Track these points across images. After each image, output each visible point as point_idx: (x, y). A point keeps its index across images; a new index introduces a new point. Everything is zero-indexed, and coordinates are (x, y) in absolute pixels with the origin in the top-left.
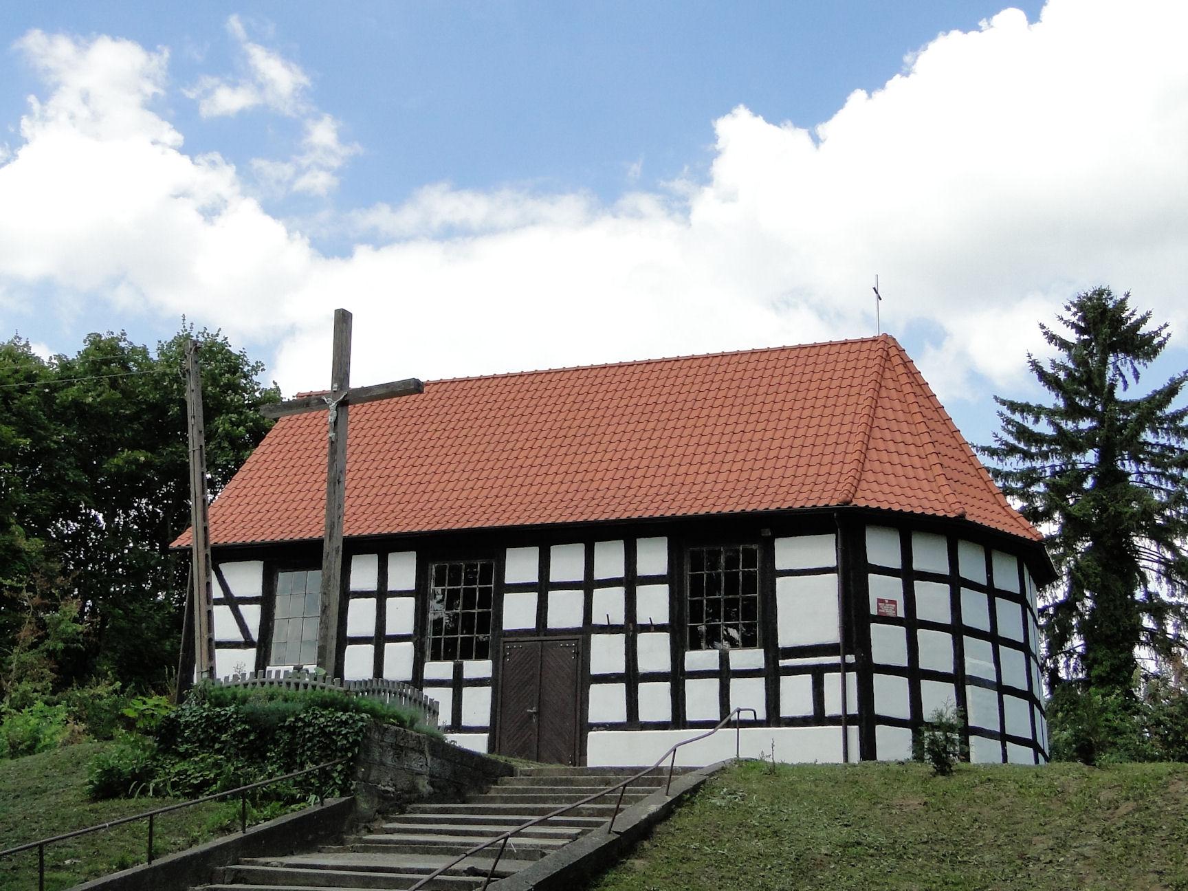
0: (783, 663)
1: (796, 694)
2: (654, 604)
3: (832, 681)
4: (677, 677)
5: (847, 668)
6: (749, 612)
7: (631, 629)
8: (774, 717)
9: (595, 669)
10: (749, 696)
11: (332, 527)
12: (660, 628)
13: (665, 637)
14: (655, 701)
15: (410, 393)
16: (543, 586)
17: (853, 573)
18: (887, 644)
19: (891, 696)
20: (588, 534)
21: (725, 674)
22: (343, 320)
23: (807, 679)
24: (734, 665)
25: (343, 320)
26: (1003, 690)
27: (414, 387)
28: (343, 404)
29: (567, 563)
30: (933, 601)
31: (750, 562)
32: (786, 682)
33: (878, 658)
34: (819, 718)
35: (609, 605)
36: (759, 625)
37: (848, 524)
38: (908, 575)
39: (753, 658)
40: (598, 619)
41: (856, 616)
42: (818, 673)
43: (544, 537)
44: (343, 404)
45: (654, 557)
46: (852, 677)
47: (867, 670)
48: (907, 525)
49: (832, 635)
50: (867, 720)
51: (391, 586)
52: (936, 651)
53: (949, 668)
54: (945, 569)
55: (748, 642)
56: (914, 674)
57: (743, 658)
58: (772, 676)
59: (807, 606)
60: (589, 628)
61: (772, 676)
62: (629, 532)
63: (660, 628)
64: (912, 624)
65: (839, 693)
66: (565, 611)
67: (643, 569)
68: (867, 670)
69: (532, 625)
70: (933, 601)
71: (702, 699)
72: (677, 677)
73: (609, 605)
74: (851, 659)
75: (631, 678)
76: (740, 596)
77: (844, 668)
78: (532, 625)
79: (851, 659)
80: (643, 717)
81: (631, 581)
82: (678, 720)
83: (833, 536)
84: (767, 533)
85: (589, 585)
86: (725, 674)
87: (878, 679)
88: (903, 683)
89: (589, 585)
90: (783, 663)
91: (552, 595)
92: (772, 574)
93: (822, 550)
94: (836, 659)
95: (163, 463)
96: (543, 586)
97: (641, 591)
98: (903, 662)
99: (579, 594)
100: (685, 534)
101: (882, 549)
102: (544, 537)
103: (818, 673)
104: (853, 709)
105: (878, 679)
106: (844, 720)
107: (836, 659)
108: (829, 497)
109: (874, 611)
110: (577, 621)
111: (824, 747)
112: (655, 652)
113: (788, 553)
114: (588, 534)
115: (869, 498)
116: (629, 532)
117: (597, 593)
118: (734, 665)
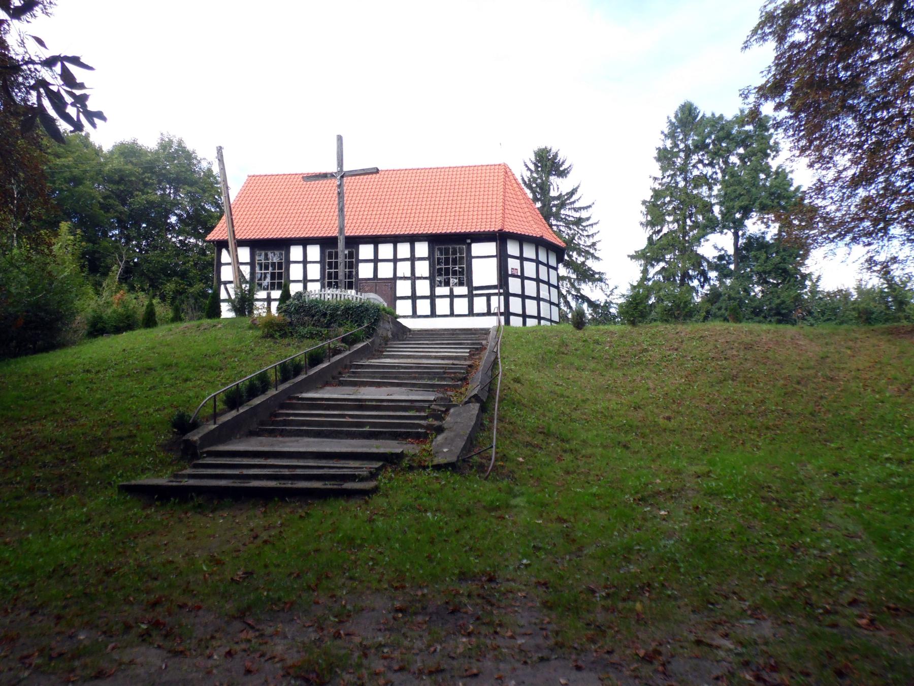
0: (475, 292)
1: (480, 304)
2: (423, 268)
3: (494, 300)
4: (432, 297)
5: (501, 294)
6: (461, 273)
7: (413, 278)
8: (471, 313)
9: (398, 295)
10: (461, 306)
11: (341, 230)
12: (425, 278)
13: (427, 282)
14: (424, 307)
15: (372, 173)
16: (376, 261)
17: (502, 257)
18: (514, 285)
19: (515, 305)
20: (395, 240)
21: (452, 296)
22: (340, 139)
23: (485, 298)
24: (455, 293)
25: (340, 139)
26: (551, 303)
27: (377, 171)
28: (342, 177)
29: (386, 250)
30: (530, 269)
31: (461, 252)
32: (476, 299)
33: (511, 291)
34: (489, 313)
35: (404, 269)
36: (465, 277)
37: (501, 238)
38: (522, 259)
39: (464, 290)
40: (399, 274)
41: (503, 274)
42: (488, 296)
43: (376, 240)
44: (342, 177)
45: (422, 249)
46: (502, 298)
47: (507, 295)
48: (522, 239)
49: (494, 282)
50: (507, 314)
51: (399, 257)
52: (531, 288)
53: (535, 295)
54: (534, 257)
55: (461, 284)
56: (523, 297)
57: (458, 290)
58: (471, 297)
59: (484, 271)
60: (395, 278)
61: (471, 297)
62: (412, 239)
63: (425, 278)
64: (523, 278)
65: (496, 303)
66: (385, 271)
67: (418, 254)
68: (507, 295)
69: (371, 276)
70: (530, 269)
71: (442, 306)
72: (432, 297)
73: (404, 269)
74: (502, 291)
75: (414, 298)
76: (450, 266)
77: (499, 294)
78: (371, 276)
79: (502, 291)
80: (419, 313)
81: (413, 259)
82: (433, 314)
83: (494, 244)
84: (469, 241)
85: (395, 260)
86: (452, 296)
87: (511, 298)
88: (520, 300)
89: (395, 260)
90: (475, 292)
91: (380, 264)
92: (470, 258)
93: (490, 248)
94: (496, 291)
95: (768, 214)
96: (376, 261)
97: (417, 263)
98: (520, 292)
99: (392, 264)
100: (434, 240)
101: (513, 248)
102: (376, 240)
103: (488, 296)
104: (502, 310)
105: (511, 298)
106: (502, 314)
107: (496, 291)
108: (494, 227)
109: (510, 273)
110: (391, 276)
111: (490, 323)
112: (423, 288)
113: (478, 249)
114: (395, 240)
115: (509, 228)
116: (412, 239)
117: (399, 264)
118: (455, 293)
